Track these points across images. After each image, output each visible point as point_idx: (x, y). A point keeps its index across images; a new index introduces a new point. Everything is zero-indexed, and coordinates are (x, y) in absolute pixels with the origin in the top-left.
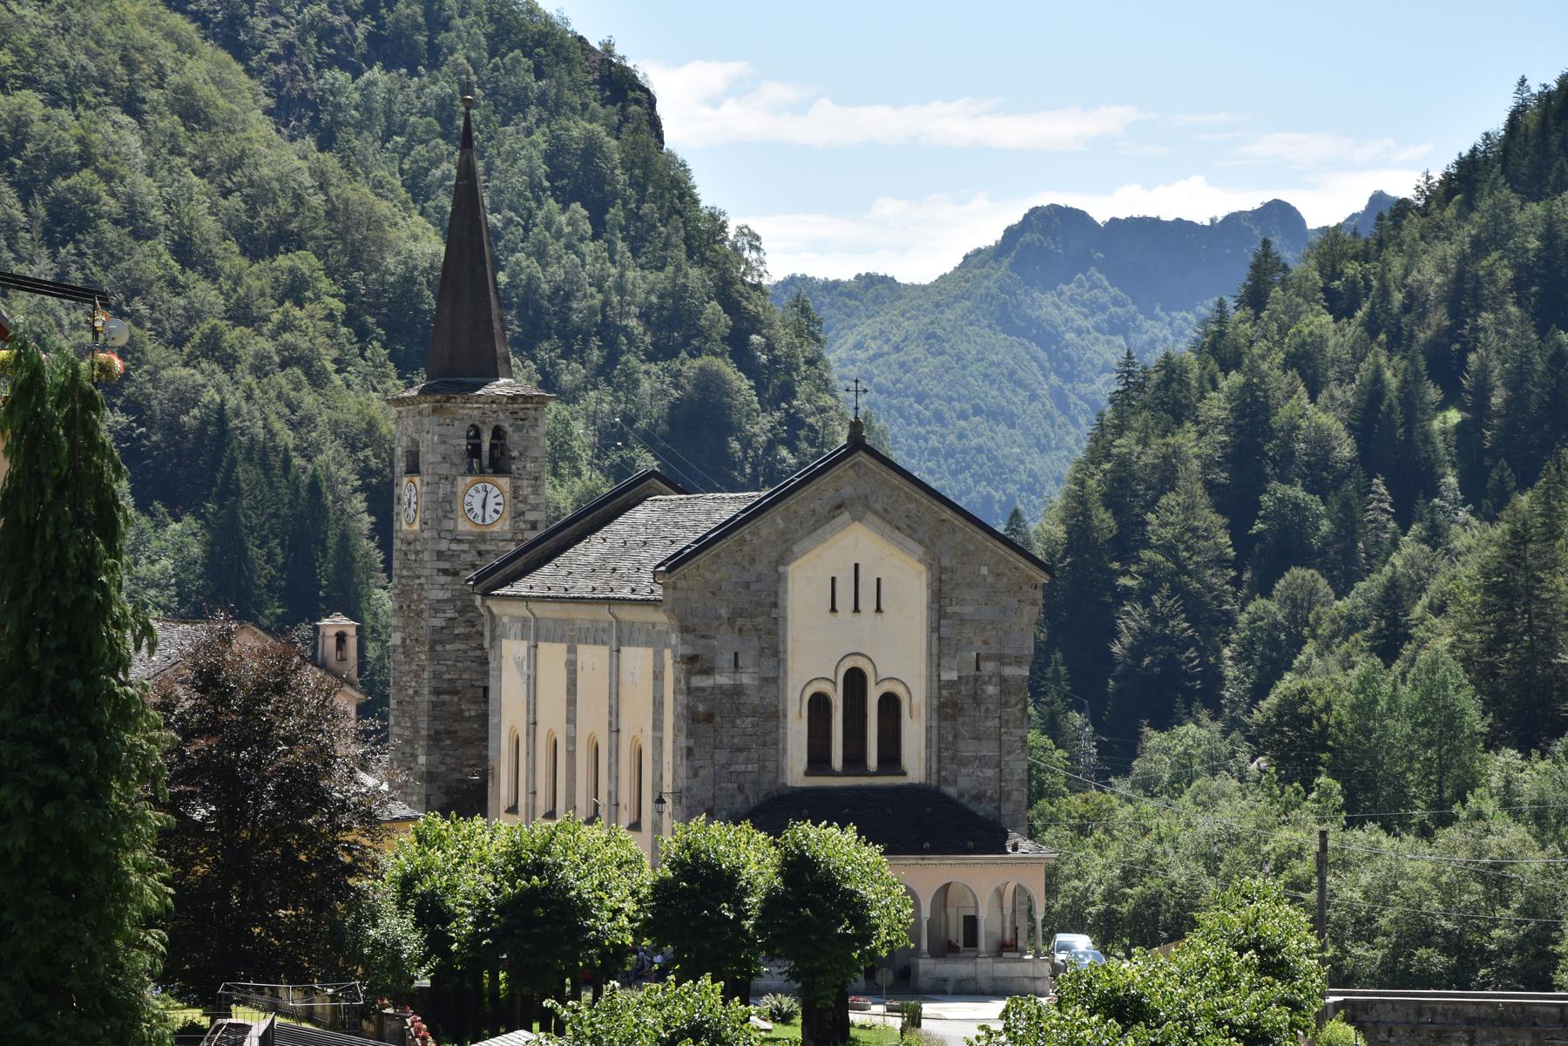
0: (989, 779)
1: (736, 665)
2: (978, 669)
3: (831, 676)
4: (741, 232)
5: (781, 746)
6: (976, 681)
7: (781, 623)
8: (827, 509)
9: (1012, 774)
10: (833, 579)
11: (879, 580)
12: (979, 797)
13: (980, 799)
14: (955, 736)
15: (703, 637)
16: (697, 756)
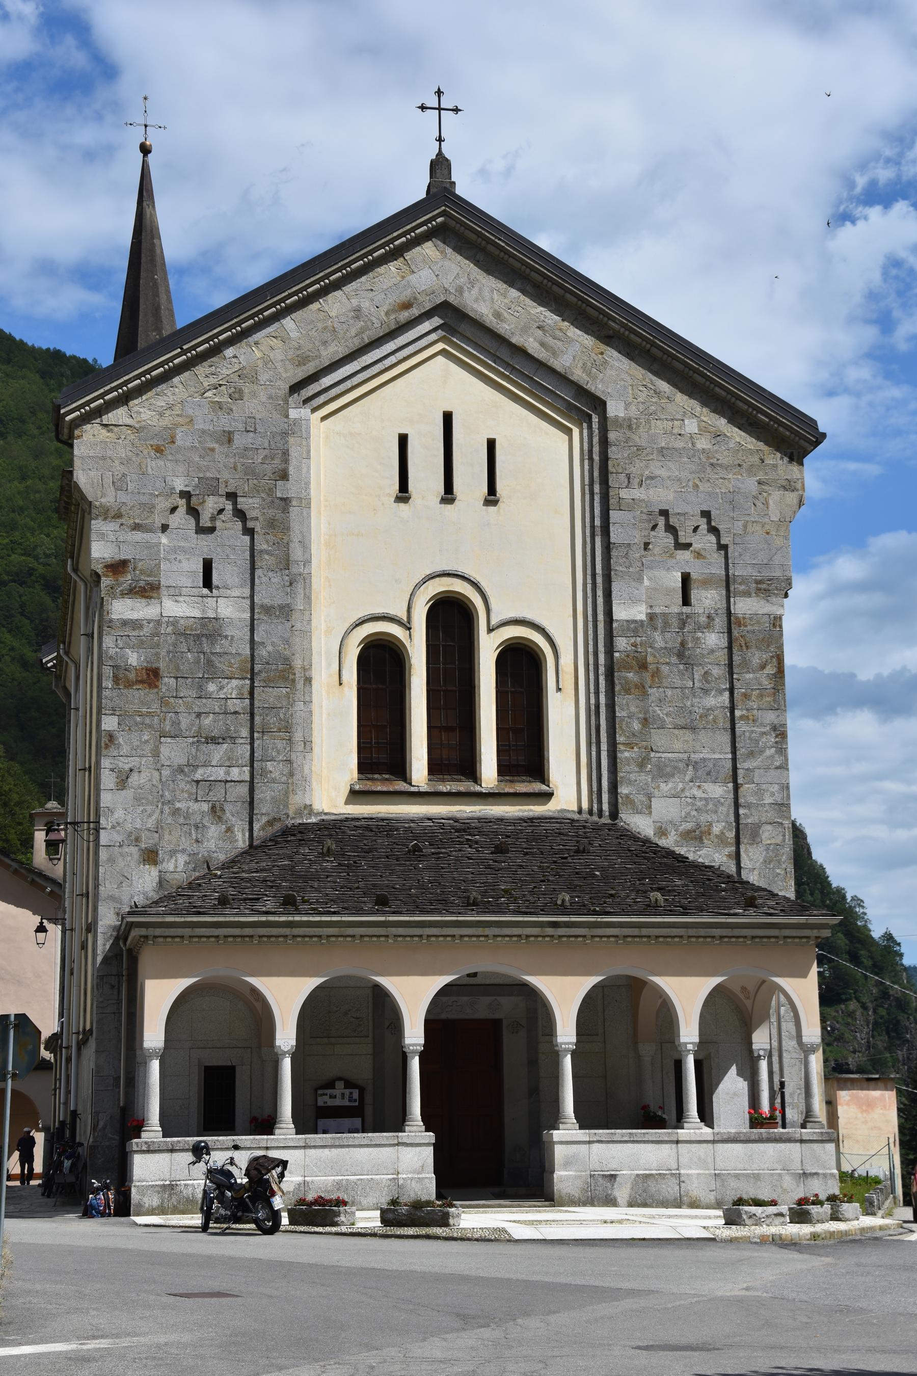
0: (718, 802)
1: (208, 582)
2: (686, 601)
3: (403, 615)
4: (853, 899)
5: (298, 736)
6: (683, 623)
7: (294, 511)
8: (385, 308)
9: (759, 793)
10: (403, 440)
11: (491, 445)
12: (696, 836)
13: (700, 839)
14: (645, 722)
15: (136, 527)
16: (125, 750)
